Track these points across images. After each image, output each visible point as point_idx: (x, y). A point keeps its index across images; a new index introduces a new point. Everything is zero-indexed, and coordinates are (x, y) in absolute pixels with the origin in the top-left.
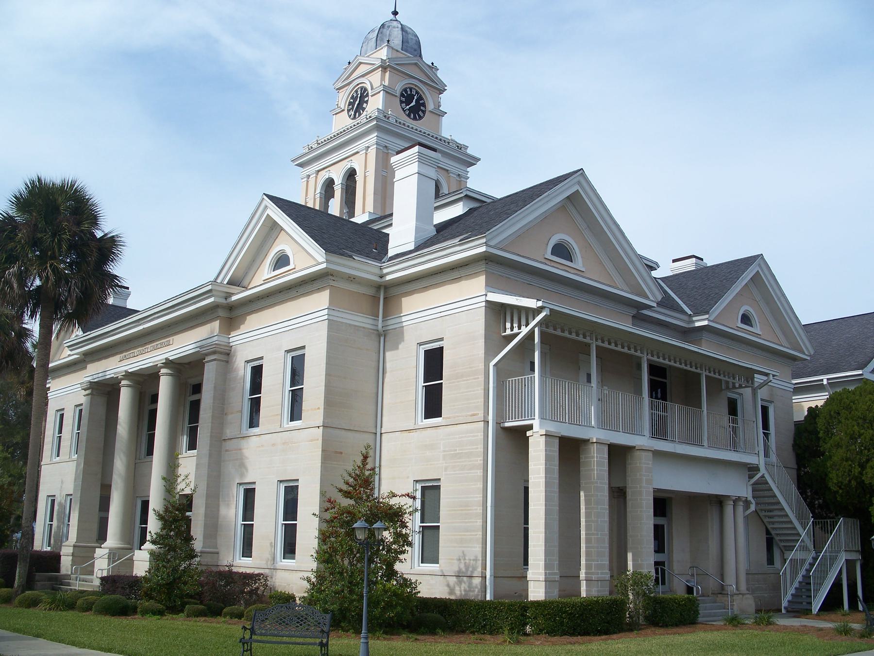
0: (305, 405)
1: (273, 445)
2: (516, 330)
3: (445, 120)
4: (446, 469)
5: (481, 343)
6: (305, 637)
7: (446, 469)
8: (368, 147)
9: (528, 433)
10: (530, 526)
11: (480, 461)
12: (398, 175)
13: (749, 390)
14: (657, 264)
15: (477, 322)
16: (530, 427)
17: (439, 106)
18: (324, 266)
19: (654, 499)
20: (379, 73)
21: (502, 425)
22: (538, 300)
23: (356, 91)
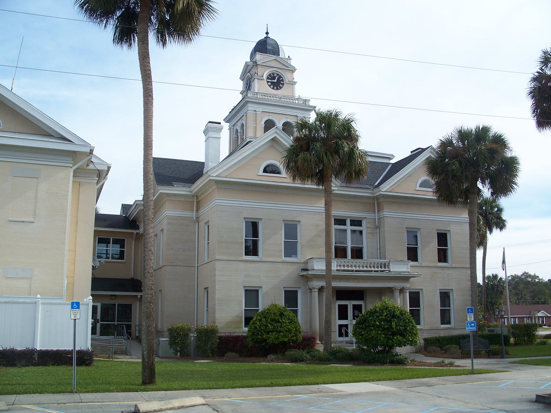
0: (52, 369)
3: (296, 86)
10: (438, 307)
14: (392, 155)
17: (293, 79)
19: (440, 293)
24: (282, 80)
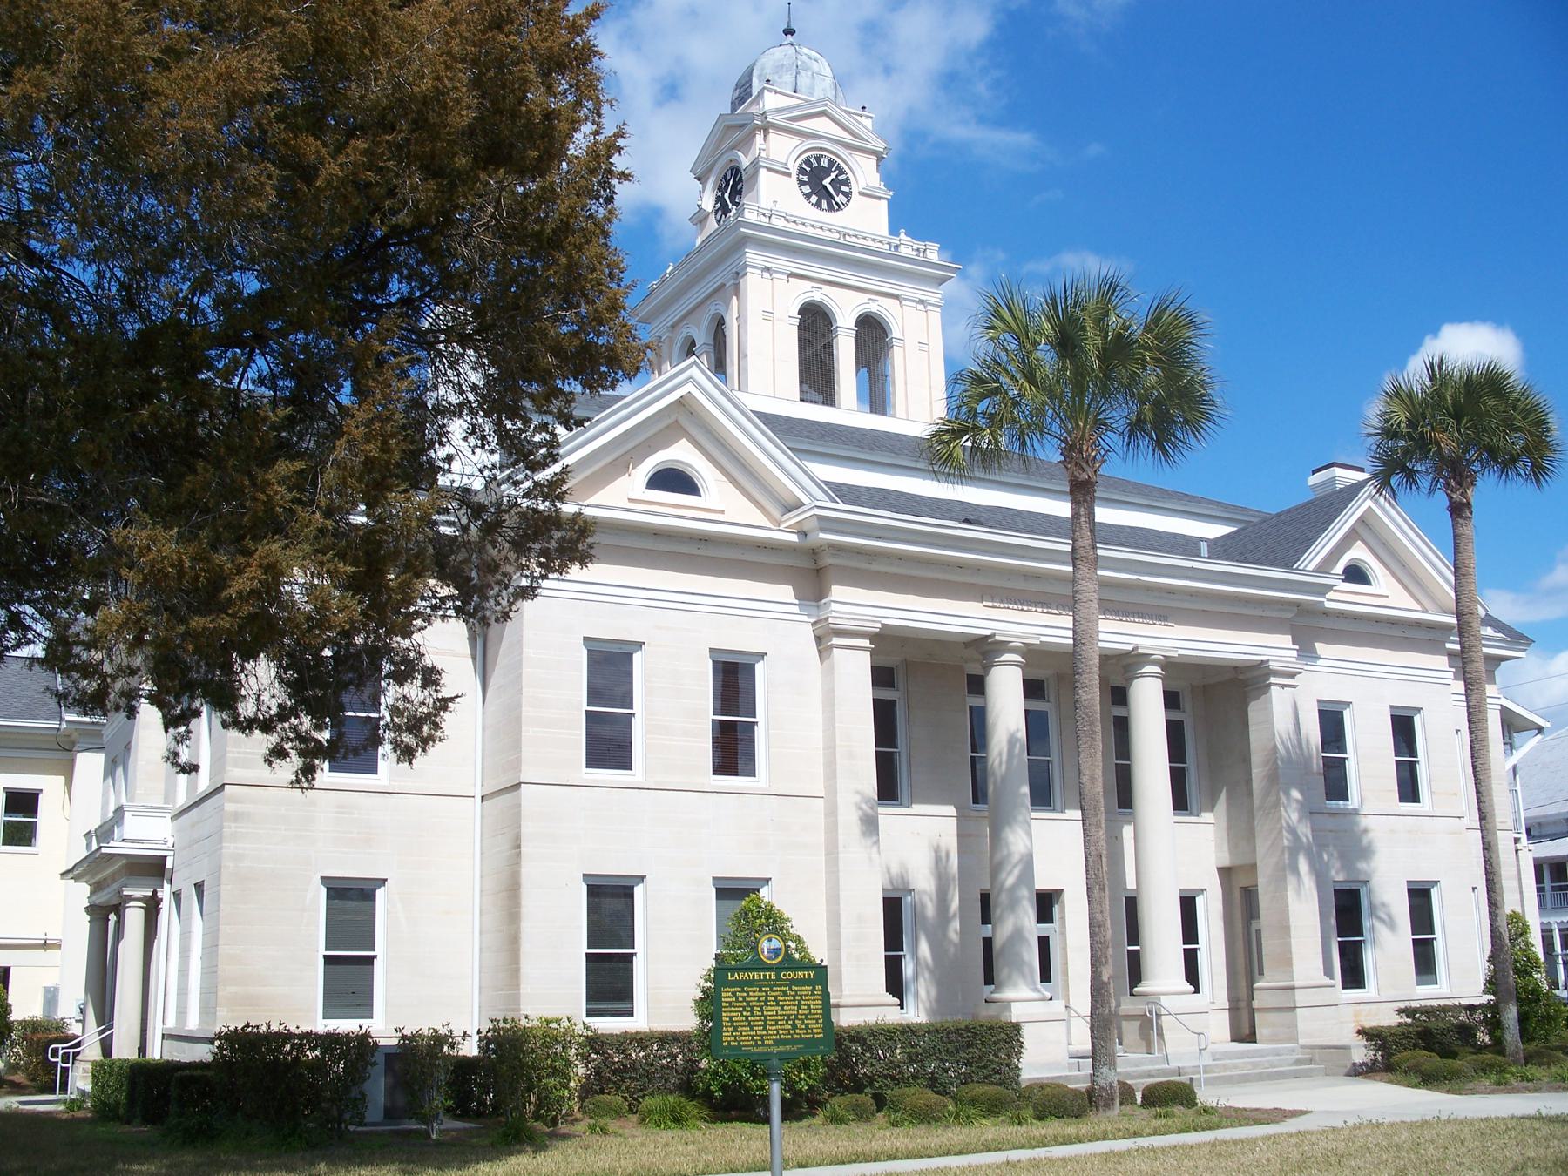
24: (847, 182)
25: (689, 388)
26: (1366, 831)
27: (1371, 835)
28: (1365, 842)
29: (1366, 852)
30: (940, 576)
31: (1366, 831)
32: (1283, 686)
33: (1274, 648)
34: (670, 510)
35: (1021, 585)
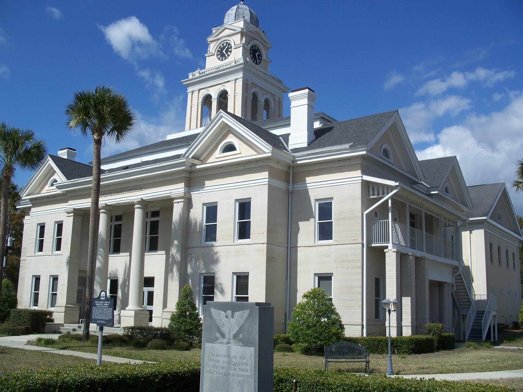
1: (228, 252)
2: (381, 195)
4: (336, 268)
5: (359, 202)
6: (354, 358)
7: (336, 268)
8: (237, 79)
9: (385, 250)
11: (360, 264)
12: (293, 104)
13: (452, 228)
15: (357, 191)
16: (387, 247)
18: (270, 154)
20: (239, 36)
21: (370, 245)
22: (396, 182)
23: (223, 45)
25: (223, 119)
26: (217, 253)
27: (219, 254)
28: (216, 257)
29: (216, 261)
30: (81, 193)
31: (217, 253)
32: (178, 202)
33: (177, 189)
34: (230, 158)
35: (118, 187)
